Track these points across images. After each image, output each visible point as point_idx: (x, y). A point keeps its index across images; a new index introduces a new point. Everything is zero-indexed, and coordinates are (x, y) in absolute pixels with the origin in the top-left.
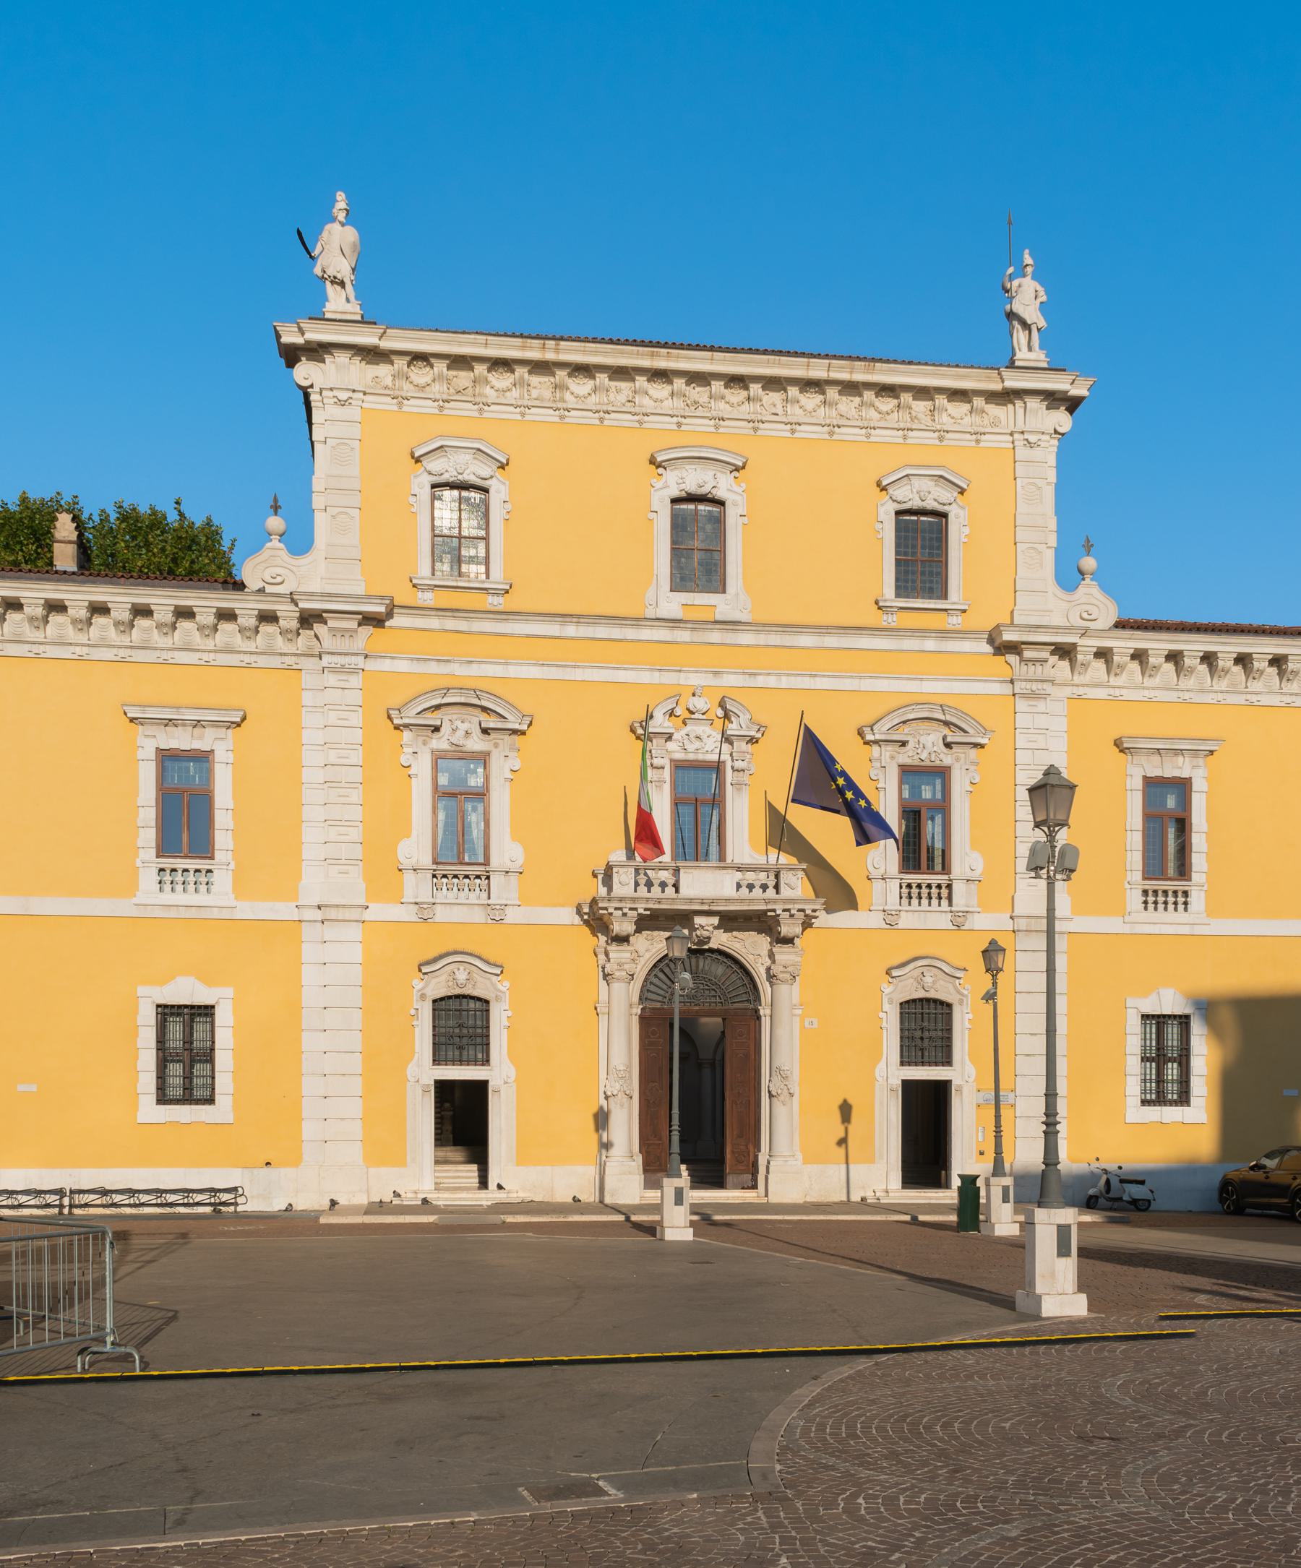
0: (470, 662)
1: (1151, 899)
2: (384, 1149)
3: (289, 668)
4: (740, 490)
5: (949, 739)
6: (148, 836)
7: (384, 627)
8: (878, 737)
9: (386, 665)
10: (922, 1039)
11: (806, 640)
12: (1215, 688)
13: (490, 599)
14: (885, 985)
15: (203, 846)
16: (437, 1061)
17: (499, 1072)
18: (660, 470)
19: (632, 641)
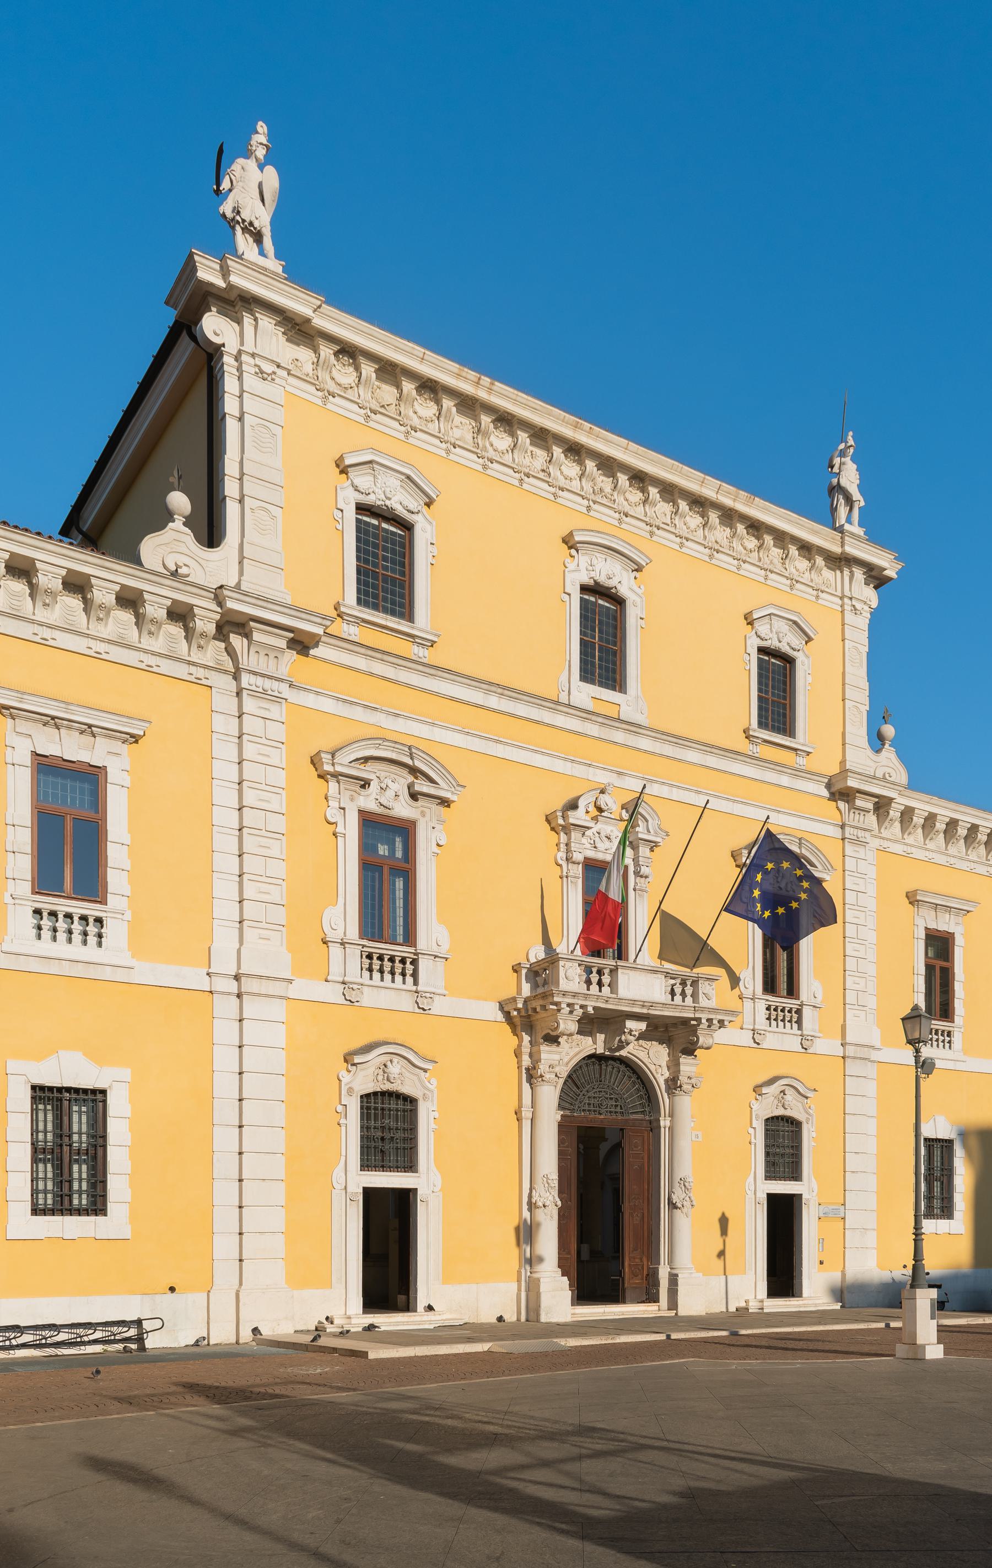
0: (397, 715)
1: (376, 964)
2: (304, 1273)
3: (197, 682)
4: (640, 591)
5: (417, 788)
6: (22, 865)
7: (307, 655)
8: (339, 769)
9: (309, 700)
10: (383, 1139)
11: (693, 756)
12: (194, 658)
13: (416, 649)
14: (343, 1073)
15: (91, 885)
16: (366, 1165)
17: (426, 1181)
18: (573, 552)
19: (548, 725)
